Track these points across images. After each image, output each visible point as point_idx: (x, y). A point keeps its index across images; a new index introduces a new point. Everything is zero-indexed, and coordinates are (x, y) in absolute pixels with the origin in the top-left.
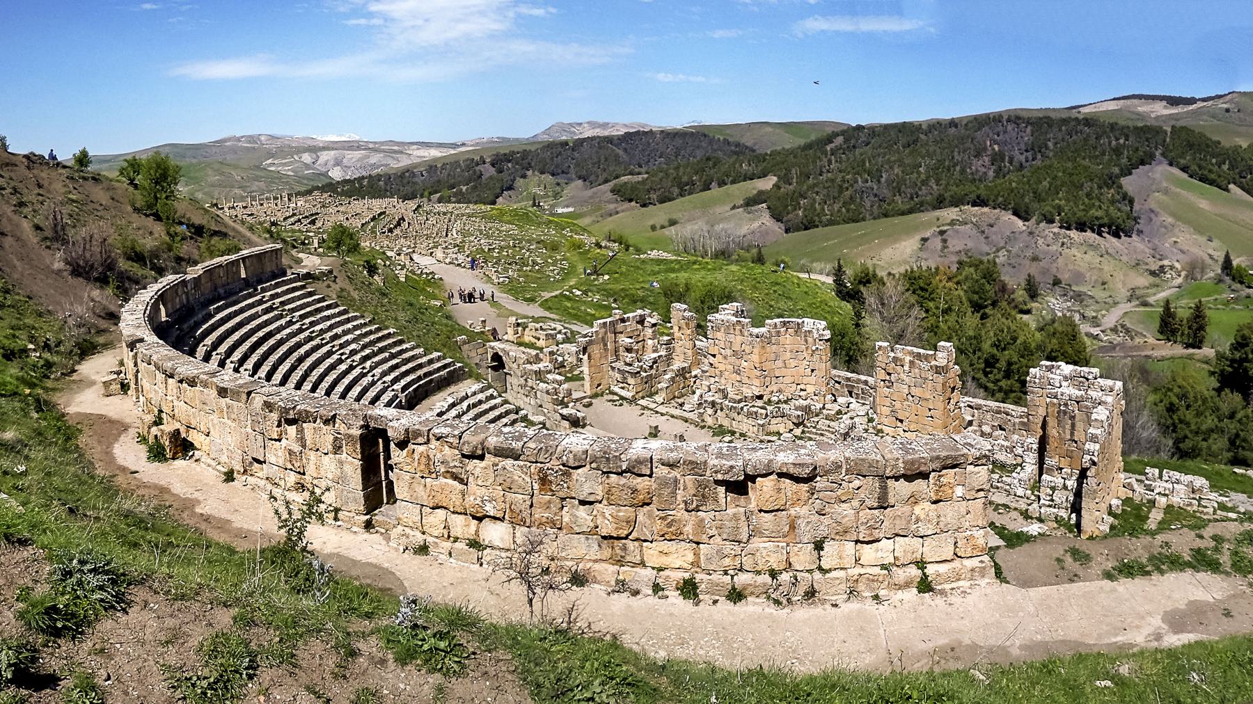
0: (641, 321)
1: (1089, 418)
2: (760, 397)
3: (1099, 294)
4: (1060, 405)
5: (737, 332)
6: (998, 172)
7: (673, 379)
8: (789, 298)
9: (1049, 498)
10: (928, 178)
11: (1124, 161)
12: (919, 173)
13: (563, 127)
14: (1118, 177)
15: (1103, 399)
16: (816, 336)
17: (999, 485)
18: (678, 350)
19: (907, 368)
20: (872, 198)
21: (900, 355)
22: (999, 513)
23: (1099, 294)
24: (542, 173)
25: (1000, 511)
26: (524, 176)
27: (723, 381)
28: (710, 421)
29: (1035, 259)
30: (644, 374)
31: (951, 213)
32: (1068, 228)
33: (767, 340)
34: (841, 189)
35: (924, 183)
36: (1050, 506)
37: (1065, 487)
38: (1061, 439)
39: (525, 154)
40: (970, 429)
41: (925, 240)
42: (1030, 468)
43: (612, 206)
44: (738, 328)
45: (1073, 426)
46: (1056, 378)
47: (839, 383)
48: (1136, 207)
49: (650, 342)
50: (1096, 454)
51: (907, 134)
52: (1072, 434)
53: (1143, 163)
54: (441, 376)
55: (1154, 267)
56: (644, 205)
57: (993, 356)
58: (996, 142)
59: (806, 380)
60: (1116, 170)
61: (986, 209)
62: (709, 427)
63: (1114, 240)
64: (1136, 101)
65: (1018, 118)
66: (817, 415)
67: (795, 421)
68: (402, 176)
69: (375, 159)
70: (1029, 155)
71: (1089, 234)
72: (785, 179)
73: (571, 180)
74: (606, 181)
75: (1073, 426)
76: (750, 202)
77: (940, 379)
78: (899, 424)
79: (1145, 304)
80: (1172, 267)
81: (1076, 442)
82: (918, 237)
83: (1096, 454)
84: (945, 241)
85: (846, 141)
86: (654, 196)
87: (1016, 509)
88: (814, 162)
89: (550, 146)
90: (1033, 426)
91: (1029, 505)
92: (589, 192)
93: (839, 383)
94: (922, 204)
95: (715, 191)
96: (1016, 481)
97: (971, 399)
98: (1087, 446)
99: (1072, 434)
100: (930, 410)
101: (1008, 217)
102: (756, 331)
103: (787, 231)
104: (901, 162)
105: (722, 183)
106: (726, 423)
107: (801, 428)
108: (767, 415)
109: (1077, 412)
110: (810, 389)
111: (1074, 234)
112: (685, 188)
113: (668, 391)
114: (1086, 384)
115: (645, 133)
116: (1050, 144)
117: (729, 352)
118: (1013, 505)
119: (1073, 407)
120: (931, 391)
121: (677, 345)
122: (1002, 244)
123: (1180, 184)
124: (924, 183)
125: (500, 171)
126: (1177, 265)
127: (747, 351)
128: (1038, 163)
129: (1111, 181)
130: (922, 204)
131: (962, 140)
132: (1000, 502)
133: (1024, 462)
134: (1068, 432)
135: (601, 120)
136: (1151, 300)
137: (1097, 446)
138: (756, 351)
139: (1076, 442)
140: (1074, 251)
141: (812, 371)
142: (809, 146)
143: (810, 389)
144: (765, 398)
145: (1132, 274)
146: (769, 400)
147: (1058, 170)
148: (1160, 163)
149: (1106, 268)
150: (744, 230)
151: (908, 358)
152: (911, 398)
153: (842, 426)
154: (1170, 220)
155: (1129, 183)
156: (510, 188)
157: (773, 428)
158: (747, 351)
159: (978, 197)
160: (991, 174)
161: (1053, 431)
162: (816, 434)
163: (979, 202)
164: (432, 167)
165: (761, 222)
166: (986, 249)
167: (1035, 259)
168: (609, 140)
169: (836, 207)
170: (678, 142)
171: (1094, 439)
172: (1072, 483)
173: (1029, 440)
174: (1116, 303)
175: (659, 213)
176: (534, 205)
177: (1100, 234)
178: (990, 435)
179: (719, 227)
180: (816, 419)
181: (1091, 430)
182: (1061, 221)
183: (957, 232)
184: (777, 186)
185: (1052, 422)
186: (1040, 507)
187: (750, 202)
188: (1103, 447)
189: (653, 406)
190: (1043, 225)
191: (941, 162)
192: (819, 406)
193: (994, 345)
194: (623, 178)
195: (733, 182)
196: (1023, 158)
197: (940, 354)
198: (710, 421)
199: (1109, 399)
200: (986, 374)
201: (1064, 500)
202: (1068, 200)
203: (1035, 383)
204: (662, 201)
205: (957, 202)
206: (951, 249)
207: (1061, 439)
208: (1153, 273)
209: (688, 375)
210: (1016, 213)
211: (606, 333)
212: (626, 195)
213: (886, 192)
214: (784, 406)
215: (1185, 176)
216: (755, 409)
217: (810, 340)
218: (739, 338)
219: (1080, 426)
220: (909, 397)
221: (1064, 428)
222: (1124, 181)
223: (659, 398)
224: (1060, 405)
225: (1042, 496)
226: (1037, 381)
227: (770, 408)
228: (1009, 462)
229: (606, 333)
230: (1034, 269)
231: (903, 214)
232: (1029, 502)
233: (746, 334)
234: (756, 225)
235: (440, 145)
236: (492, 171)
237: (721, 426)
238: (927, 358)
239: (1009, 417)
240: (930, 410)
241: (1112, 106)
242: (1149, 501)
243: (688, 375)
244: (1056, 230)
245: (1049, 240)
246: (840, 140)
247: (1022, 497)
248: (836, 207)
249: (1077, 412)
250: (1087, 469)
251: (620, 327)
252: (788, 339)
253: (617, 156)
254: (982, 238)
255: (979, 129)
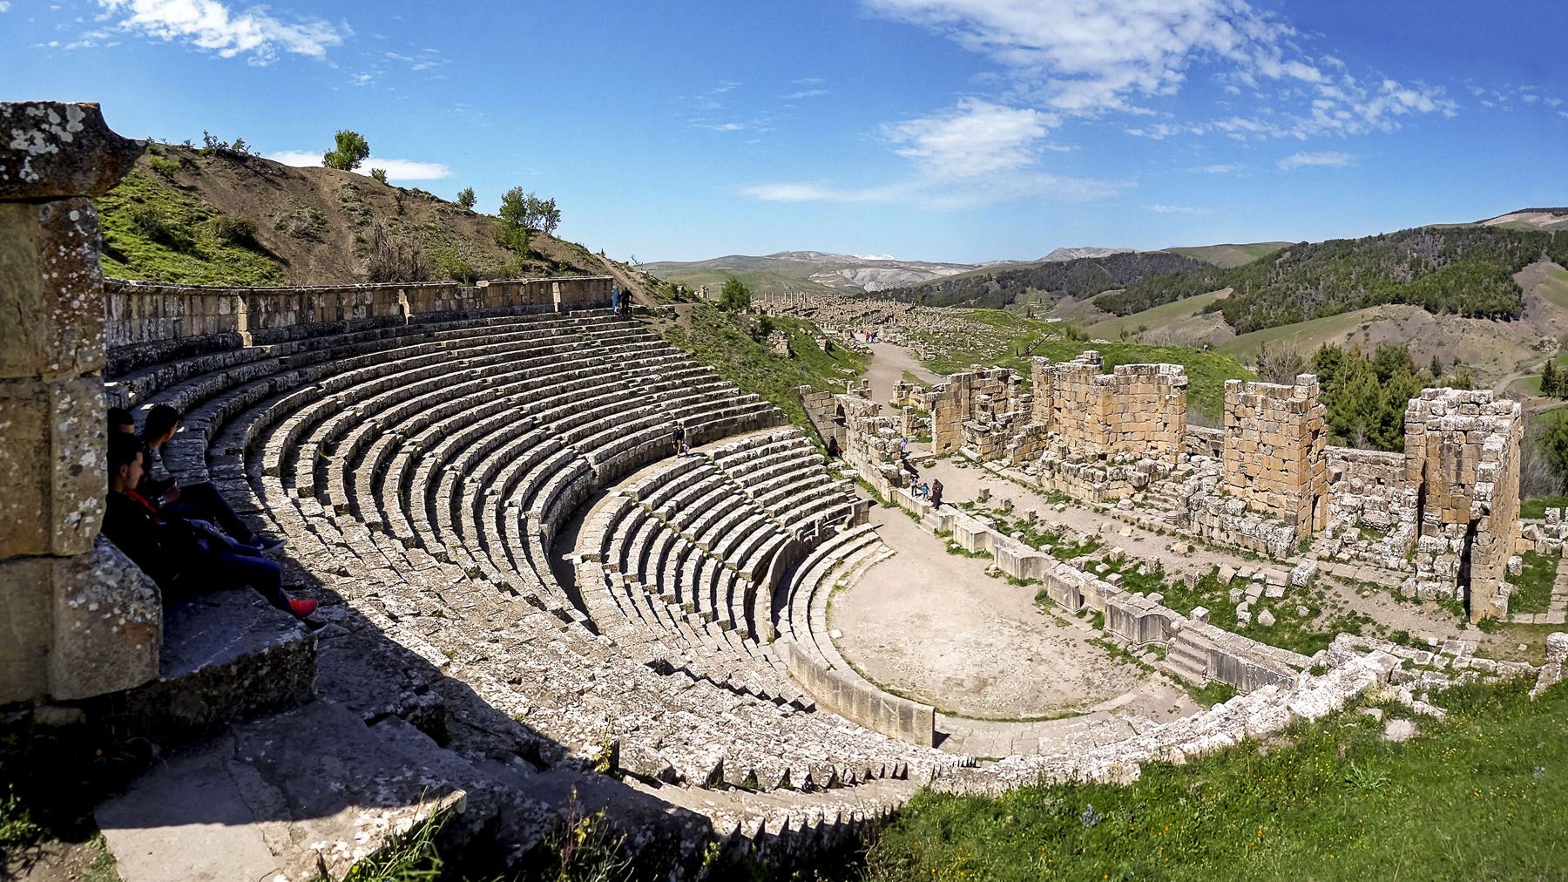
0: (1004, 378)
1: (1479, 450)
2: (1103, 457)
3: (1492, 369)
4: (1444, 439)
5: (1083, 380)
6: (1415, 275)
7: (1023, 440)
8: (1207, 376)
9: (1427, 568)
10: (1357, 283)
11: (1516, 260)
12: (1350, 279)
13: (1063, 251)
14: (1511, 273)
15: (1498, 424)
16: (1170, 382)
17: (1367, 555)
18: (1037, 408)
19: (1258, 409)
20: (1310, 302)
21: (1251, 393)
22: (1364, 597)
23: (1492, 369)
24: (1040, 289)
25: (1365, 593)
26: (1024, 292)
27: (1067, 439)
28: (1047, 486)
29: (1440, 344)
30: (995, 434)
31: (1374, 311)
32: (1469, 317)
33: (1112, 389)
34: (1285, 296)
35: (1353, 288)
36: (1430, 579)
37: (1450, 550)
38: (1444, 484)
39: (1027, 272)
40: (1337, 484)
41: (1351, 335)
42: (1407, 528)
43: (1093, 317)
44: (1083, 375)
45: (1459, 464)
46: (1440, 402)
47: (1205, 441)
48: (1524, 296)
49: (1012, 401)
50: (1488, 498)
51: (1342, 249)
52: (1458, 476)
53: (1531, 261)
54: (439, 411)
55: (1536, 343)
56: (1120, 316)
57: (1389, 414)
58: (1415, 251)
59: (1158, 436)
60: (1510, 268)
61: (1403, 306)
62: (1046, 493)
63: (1505, 323)
64: (1530, 214)
65: (1434, 229)
66: (1165, 477)
67: (1136, 484)
68: (921, 290)
69: (905, 276)
70: (1441, 260)
71: (1485, 319)
72: (1240, 290)
73: (1064, 295)
74: (1091, 295)
75: (1459, 464)
76: (1208, 310)
77: (1297, 420)
78: (1249, 482)
79: (1528, 373)
80: (1550, 342)
81: (1463, 486)
82: (1345, 333)
83: (1488, 498)
84: (1367, 335)
85: (1293, 255)
86: (1129, 307)
87: (1386, 588)
88: (1265, 275)
89: (1048, 265)
90: (1412, 473)
91: (1403, 580)
92: (1076, 305)
93: (1205, 441)
94: (1350, 305)
95: (1181, 301)
96: (1387, 548)
97: (1346, 450)
98: (1477, 488)
99: (1458, 476)
100: (1284, 461)
101: (1420, 311)
102: (1101, 377)
103: (1238, 334)
104: (1336, 271)
105: (1187, 295)
106: (1062, 487)
107: (1143, 493)
108: (1105, 478)
109: (1464, 445)
110: (1162, 447)
111: (1473, 321)
112: (1155, 300)
113: (1017, 452)
114: (1477, 410)
115: (1128, 255)
116: (1459, 250)
117: (1073, 405)
118: (1382, 583)
119: (1460, 439)
120: (1287, 439)
121: (1036, 402)
122: (1414, 334)
123: (1558, 275)
124: (1353, 288)
125: (1004, 287)
126: (1554, 340)
127: (1092, 402)
128: (1448, 266)
129: (1505, 277)
130: (1350, 305)
131: (1388, 250)
132: (1365, 580)
133: (1400, 520)
134: (1453, 474)
135: (1096, 246)
136: (1533, 369)
137: (1491, 487)
138: (1100, 401)
139: (1463, 486)
140: (1472, 335)
141: (1165, 425)
142: (1261, 262)
143: (1162, 447)
144: (1109, 458)
145: (1518, 349)
146: (1113, 461)
147: (1463, 270)
148: (1544, 260)
149: (1497, 346)
150: (1201, 333)
151: (1261, 396)
152: (1262, 448)
153: (1187, 489)
154: (1550, 304)
155: (1518, 278)
156: (1011, 302)
157: (1112, 494)
158: (1092, 402)
159: (1397, 296)
160: (1409, 278)
161: (1434, 476)
162: (1159, 500)
163: (1398, 300)
164: (947, 282)
165: (1217, 325)
166: (1401, 339)
167: (1440, 344)
168: (1098, 261)
169: (1280, 311)
170: (1155, 261)
171: (1486, 477)
172: (1458, 543)
173: (1407, 492)
174: (1504, 375)
175: (1131, 322)
176: (1028, 316)
177: (1494, 320)
178: (1361, 490)
179: (1179, 332)
180: (1161, 482)
181: (1483, 466)
182: (1463, 312)
183: (1378, 326)
184: (1232, 296)
185: (1433, 464)
186: (1417, 582)
187: (1208, 310)
188: (1497, 489)
189: (997, 468)
190: (1449, 315)
191: (1369, 270)
192: (1169, 466)
193: (1390, 403)
194: (1105, 293)
195: (1196, 294)
196: (1435, 263)
197: (1299, 389)
198: (1047, 486)
199: (1506, 423)
200: (1381, 432)
201: (1448, 568)
202: (1469, 294)
203: (1415, 416)
204: (1135, 312)
205: (1379, 302)
206: (1372, 341)
207: (1444, 484)
208: (1535, 348)
209: (1043, 436)
210: (1427, 308)
211: (959, 388)
212: (1105, 306)
213: (1321, 297)
214: (1129, 467)
215: (1563, 269)
216: (1092, 471)
217: (1164, 387)
218: (1084, 387)
219: (1468, 463)
220: (1261, 446)
221: (1448, 469)
222: (1515, 276)
223: (1005, 462)
224: (1444, 439)
225: (1420, 566)
226: (1417, 413)
227: (1110, 469)
228: (1381, 522)
229: (959, 388)
230: (1436, 351)
231: (1335, 314)
232: (1404, 575)
233: (1091, 381)
234: (1212, 329)
235: (961, 266)
236: (998, 286)
237: (1058, 491)
238: (1281, 393)
239: (1388, 468)
240: (1284, 461)
241: (1511, 219)
242: (1554, 551)
243: (1043, 436)
244: (1459, 319)
245: (1453, 328)
246: (1288, 254)
247: (1395, 569)
248: (1280, 311)
249: (1464, 445)
250: (1478, 521)
251: (977, 382)
252: (1139, 387)
253: (1103, 274)
254: (1398, 330)
255: (1402, 240)
